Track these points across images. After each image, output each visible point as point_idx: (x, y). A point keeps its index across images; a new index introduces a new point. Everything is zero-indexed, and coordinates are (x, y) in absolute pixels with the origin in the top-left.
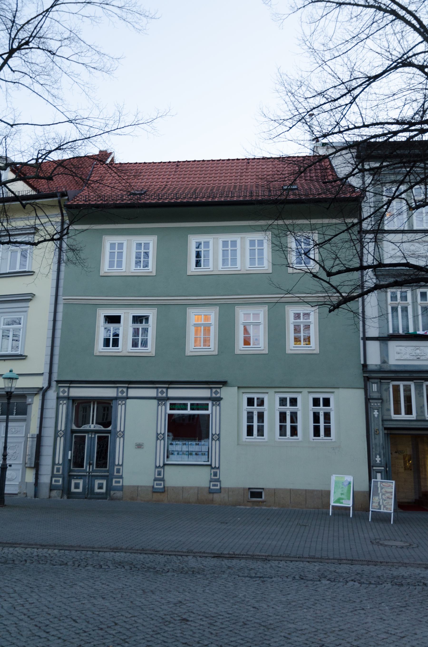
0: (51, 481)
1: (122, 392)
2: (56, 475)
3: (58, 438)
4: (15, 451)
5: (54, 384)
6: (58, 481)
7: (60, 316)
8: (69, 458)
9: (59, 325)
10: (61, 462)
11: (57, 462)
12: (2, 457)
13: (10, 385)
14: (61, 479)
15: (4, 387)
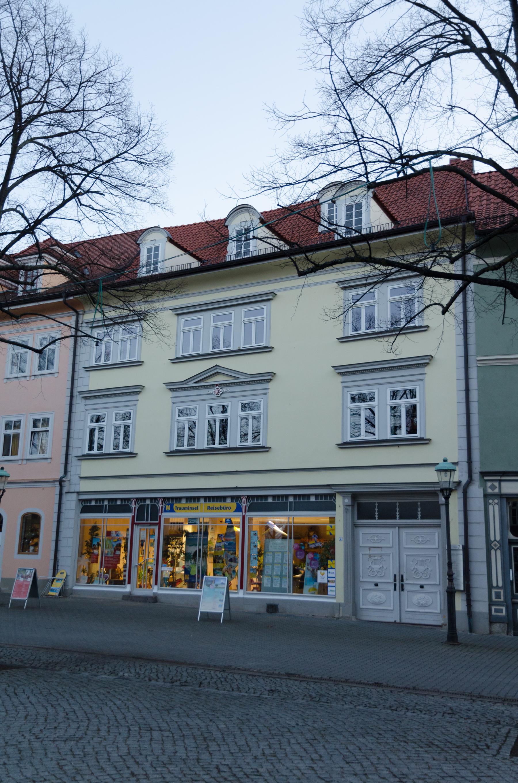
0: (490, 610)
1: (493, 487)
2: (495, 601)
3: (493, 552)
4: (426, 567)
5: (476, 476)
6: (501, 611)
7: (474, 384)
8: (511, 579)
9: (474, 396)
10: (500, 584)
11: (494, 584)
12: (447, 577)
13: (447, 479)
14: (504, 609)
15: (437, 481)
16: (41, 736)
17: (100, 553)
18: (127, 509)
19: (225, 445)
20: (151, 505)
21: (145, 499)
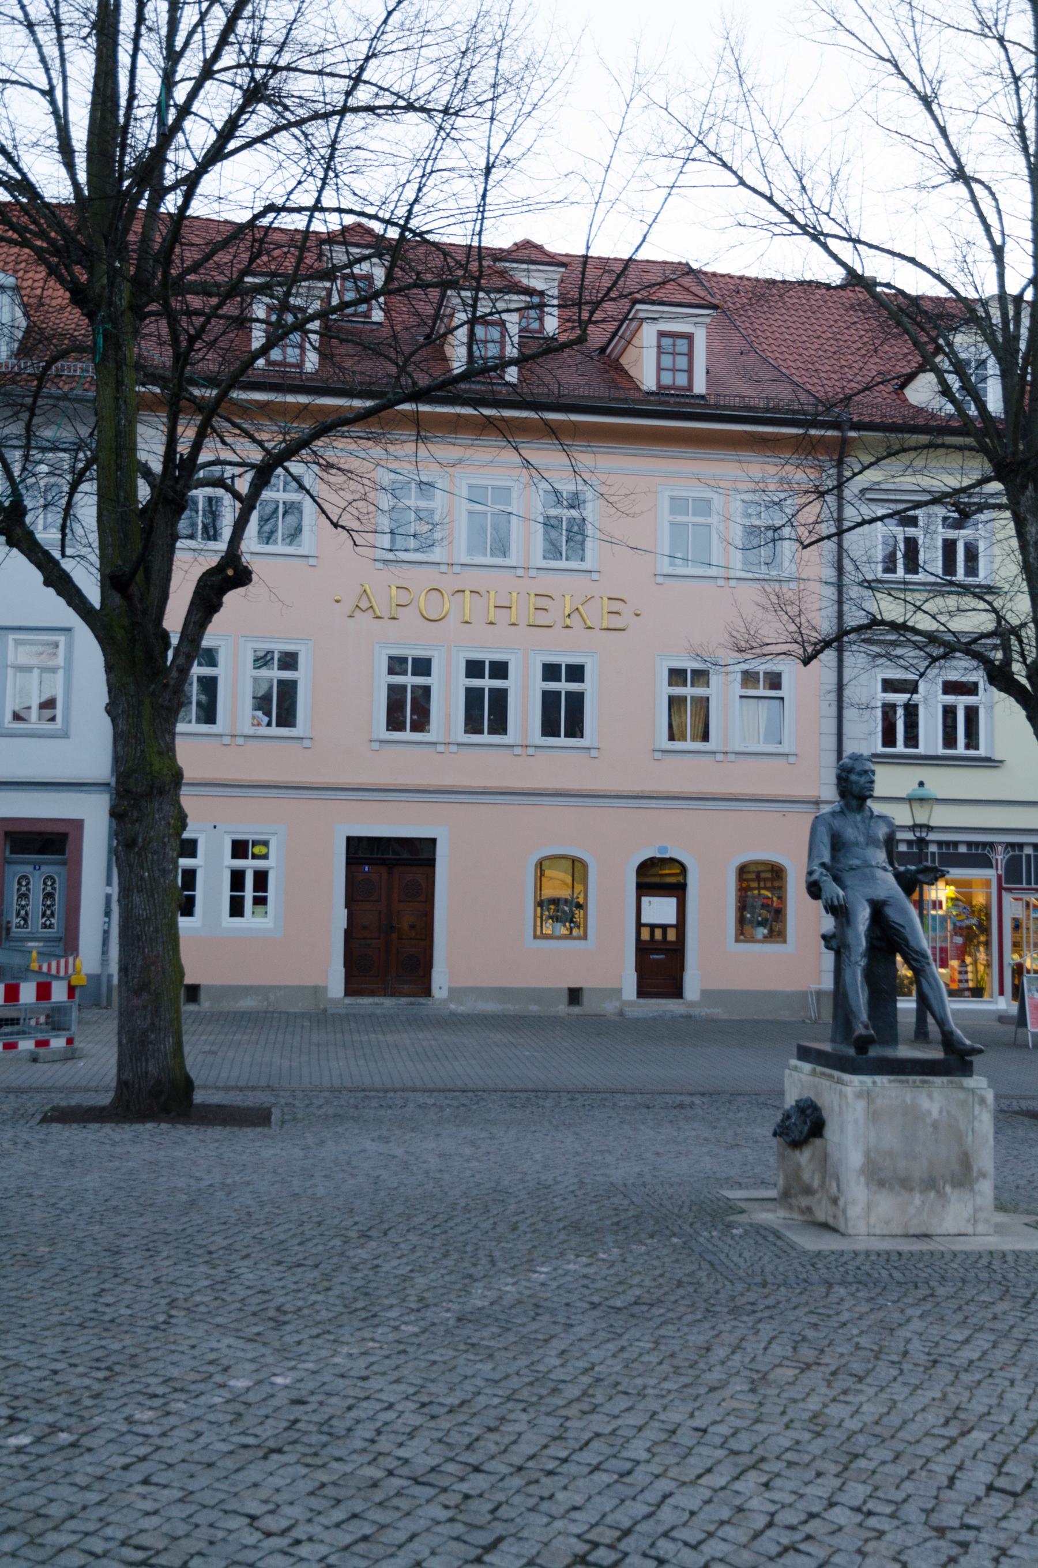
16: (803, 1285)
18: (986, 863)
20: (940, 854)
21: (1021, 846)
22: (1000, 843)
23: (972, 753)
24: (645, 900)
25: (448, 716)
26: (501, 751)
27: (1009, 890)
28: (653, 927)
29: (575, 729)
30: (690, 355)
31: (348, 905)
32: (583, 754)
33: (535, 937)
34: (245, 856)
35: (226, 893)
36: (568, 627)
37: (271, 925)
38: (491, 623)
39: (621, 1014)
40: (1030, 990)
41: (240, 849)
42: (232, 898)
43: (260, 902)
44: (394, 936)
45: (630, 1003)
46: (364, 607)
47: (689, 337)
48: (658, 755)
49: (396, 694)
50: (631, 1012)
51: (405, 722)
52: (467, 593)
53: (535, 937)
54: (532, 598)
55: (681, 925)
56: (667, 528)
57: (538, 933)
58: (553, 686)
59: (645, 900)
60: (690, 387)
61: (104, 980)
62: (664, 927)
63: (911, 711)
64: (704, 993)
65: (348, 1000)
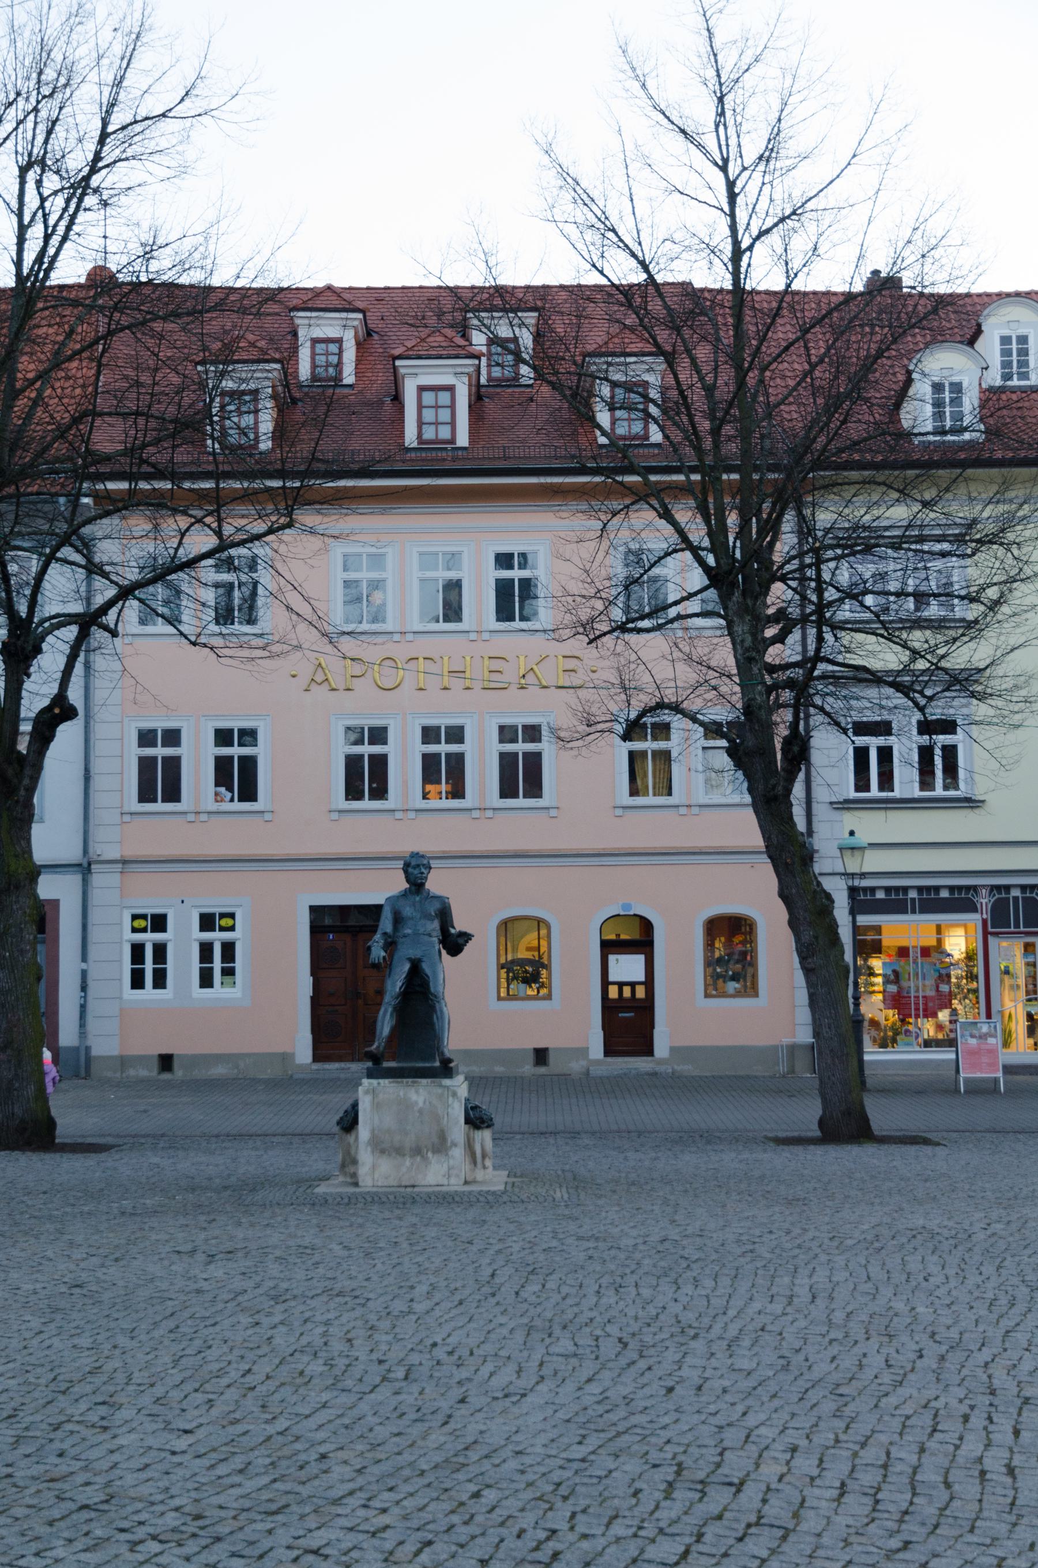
17: (912, 985)
18: (970, 907)
19: (890, 794)
21: (1007, 888)
22: (984, 886)
23: (952, 793)
24: (612, 958)
25: (405, 783)
26: (385, 816)
27: (996, 934)
28: (621, 985)
29: (534, 788)
30: (452, 407)
31: (313, 973)
32: (543, 814)
33: (499, 998)
34: (212, 929)
35: (170, 966)
36: (468, 688)
37: (239, 995)
38: (445, 689)
39: (587, 1073)
40: (962, 1036)
41: (207, 922)
42: (133, 971)
43: (228, 972)
44: (360, 1002)
45: (597, 1062)
46: (319, 680)
47: (451, 389)
48: (619, 812)
49: (146, 765)
50: (596, 1071)
51: (363, 791)
52: (421, 660)
53: (499, 998)
54: (486, 662)
55: (649, 983)
56: (416, 585)
57: (503, 994)
58: (225, 751)
59: (612, 958)
60: (453, 441)
61: (83, 1053)
62: (633, 985)
63: (886, 755)
64: (673, 1050)
65: (316, 1066)
